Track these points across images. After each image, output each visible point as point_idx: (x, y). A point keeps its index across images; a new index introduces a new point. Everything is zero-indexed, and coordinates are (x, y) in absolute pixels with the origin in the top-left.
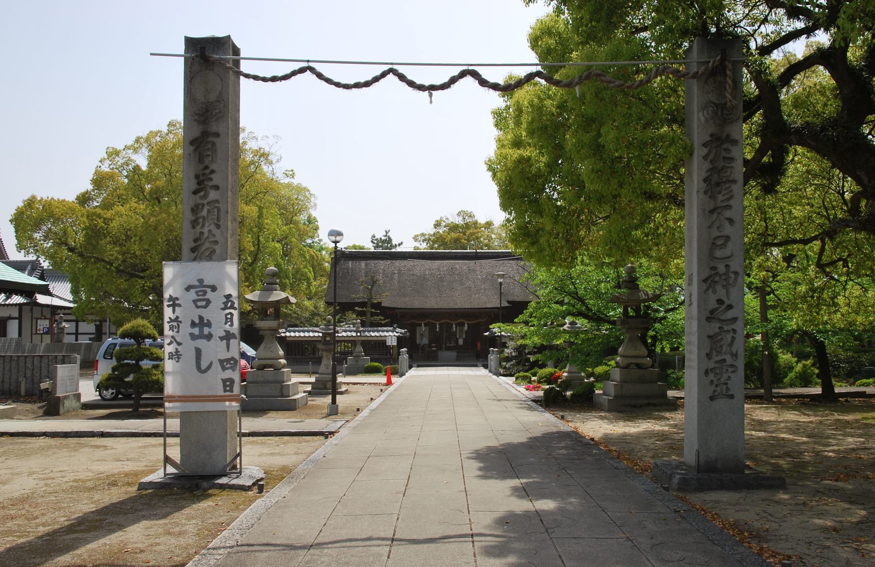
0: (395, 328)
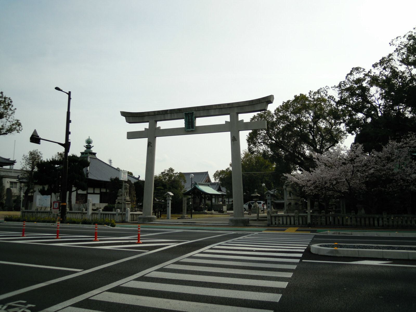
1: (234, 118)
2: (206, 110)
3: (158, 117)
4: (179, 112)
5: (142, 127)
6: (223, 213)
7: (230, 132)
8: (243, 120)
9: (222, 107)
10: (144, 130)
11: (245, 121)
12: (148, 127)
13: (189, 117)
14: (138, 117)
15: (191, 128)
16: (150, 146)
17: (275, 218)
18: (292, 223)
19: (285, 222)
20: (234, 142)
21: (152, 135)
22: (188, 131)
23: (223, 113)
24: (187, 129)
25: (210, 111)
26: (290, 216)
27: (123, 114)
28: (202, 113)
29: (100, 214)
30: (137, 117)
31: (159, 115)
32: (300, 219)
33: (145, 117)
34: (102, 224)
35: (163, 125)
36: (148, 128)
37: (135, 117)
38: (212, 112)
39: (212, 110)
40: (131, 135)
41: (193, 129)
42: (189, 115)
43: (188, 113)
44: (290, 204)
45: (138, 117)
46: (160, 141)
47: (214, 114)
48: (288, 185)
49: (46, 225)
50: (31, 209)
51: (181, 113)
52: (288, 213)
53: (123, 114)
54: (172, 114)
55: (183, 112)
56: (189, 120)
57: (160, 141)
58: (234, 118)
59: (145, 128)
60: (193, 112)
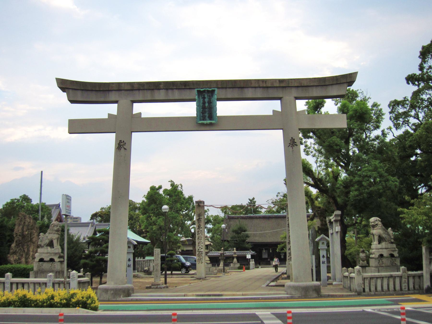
2: (239, 88)
3: (139, 95)
4: (183, 87)
6: (151, 275)
8: (140, 114)
10: (106, 117)
11: (143, 116)
12: (115, 113)
13: (204, 98)
14: (96, 91)
15: (207, 119)
16: (122, 149)
17: (393, 279)
18: (398, 287)
19: (385, 287)
21: (124, 130)
22: (203, 124)
23: (271, 96)
24: (200, 120)
25: (246, 90)
26: (393, 276)
27: (65, 85)
28: (230, 93)
29: (10, 283)
30: (92, 90)
31: (141, 91)
32: (411, 280)
33: (110, 93)
34: (31, 305)
36: (116, 114)
37: (89, 92)
38: (249, 93)
39: (250, 90)
40: (77, 127)
41: (213, 122)
42: (206, 93)
43: (204, 91)
44: (381, 256)
45: (94, 92)
46: (138, 139)
47: (254, 97)
48: (376, 224)
49: (24, 312)
50: (363, 272)
51: (188, 91)
52: (379, 272)
53: (65, 85)
54: (170, 91)
55: (195, 88)
56: (204, 103)
57: (138, 139)
59: (109, 114)
60: (213, 89)
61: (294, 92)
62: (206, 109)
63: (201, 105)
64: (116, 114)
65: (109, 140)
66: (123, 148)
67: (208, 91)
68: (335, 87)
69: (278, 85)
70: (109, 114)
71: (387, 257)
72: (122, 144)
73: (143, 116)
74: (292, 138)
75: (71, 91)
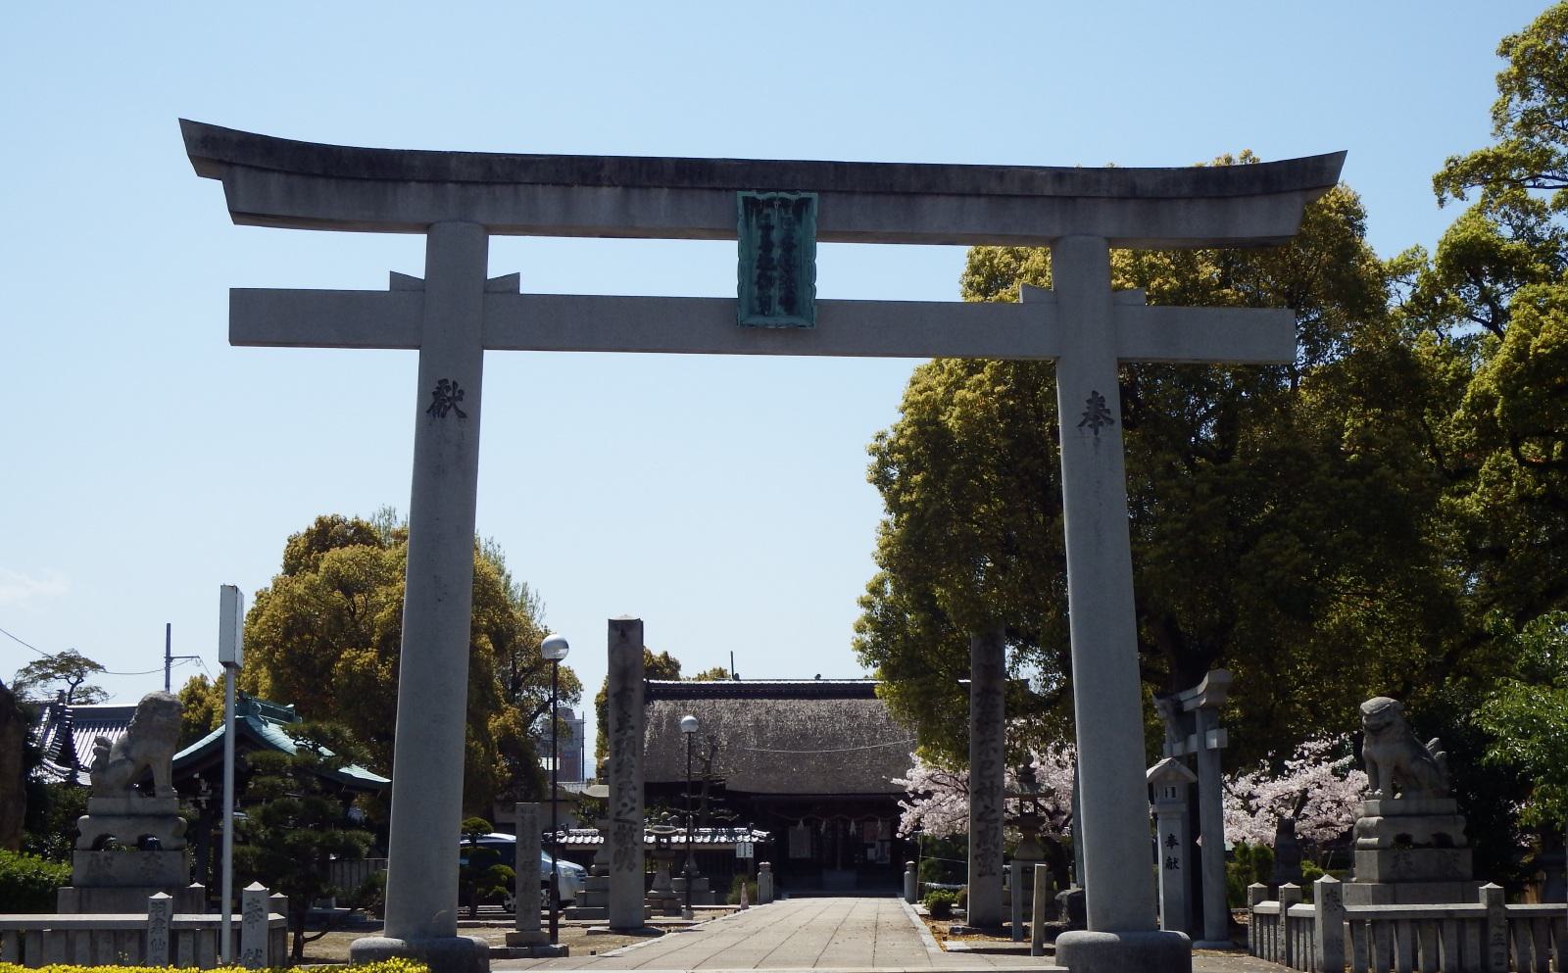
0: (750, 830)
1: (458, 258)
5: (375, 259)
7: (417, 352)
8: (514, 279)
9: (1016, 191)
10: (383, 285)
11: (525, 288)
13: (767, 229)
20: (1096, 433)
21: (452, 331)
24: (752, 312)
27: (214, 149)
35: (536, 262)
36: (422, 276)
39: (943, 203)
40: (264, 318)
41: (802, 322)
43: (770, 203)
46: (510, 379)
48: (1388, 724)
53: (214, 149)
54: (635, 193)
56: (767, 246)
57: (510, 379)
58: (458, 258)
59: (394, 276)
60: (804, 195)
61: (1106, 220)
62: (774, 268)
63: (756, 253)
64: (422, 276)
65: (392, 377)
66: (448, 417)
67: (785, 203)
68: (1262, 205)
69: (1049, 190)
70: (394, 276)
71: (1428, 845)
72: (450, 394)
73: (525, 288)
74: (1094, 393)
75: (239, 173)
